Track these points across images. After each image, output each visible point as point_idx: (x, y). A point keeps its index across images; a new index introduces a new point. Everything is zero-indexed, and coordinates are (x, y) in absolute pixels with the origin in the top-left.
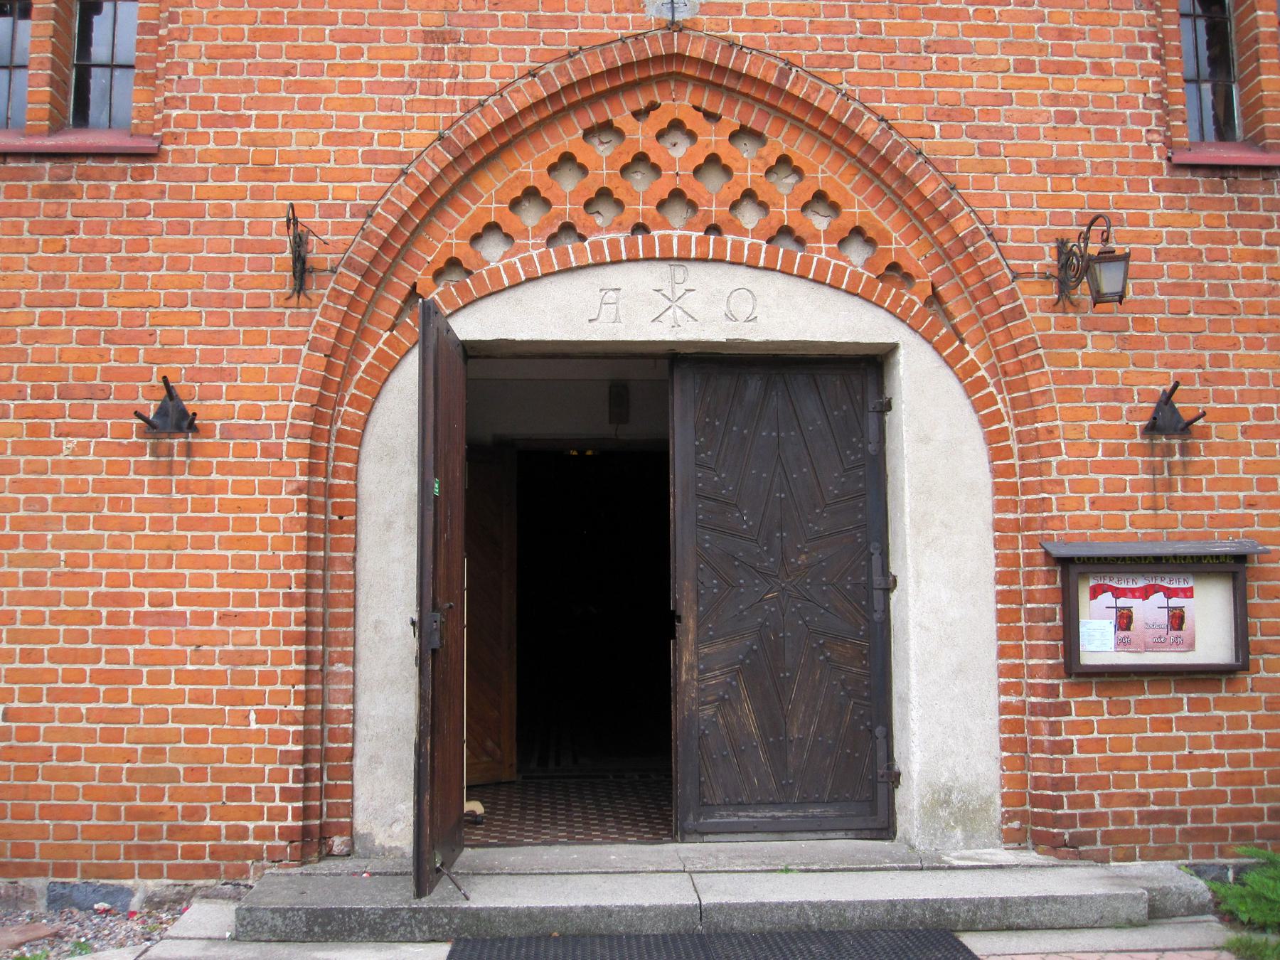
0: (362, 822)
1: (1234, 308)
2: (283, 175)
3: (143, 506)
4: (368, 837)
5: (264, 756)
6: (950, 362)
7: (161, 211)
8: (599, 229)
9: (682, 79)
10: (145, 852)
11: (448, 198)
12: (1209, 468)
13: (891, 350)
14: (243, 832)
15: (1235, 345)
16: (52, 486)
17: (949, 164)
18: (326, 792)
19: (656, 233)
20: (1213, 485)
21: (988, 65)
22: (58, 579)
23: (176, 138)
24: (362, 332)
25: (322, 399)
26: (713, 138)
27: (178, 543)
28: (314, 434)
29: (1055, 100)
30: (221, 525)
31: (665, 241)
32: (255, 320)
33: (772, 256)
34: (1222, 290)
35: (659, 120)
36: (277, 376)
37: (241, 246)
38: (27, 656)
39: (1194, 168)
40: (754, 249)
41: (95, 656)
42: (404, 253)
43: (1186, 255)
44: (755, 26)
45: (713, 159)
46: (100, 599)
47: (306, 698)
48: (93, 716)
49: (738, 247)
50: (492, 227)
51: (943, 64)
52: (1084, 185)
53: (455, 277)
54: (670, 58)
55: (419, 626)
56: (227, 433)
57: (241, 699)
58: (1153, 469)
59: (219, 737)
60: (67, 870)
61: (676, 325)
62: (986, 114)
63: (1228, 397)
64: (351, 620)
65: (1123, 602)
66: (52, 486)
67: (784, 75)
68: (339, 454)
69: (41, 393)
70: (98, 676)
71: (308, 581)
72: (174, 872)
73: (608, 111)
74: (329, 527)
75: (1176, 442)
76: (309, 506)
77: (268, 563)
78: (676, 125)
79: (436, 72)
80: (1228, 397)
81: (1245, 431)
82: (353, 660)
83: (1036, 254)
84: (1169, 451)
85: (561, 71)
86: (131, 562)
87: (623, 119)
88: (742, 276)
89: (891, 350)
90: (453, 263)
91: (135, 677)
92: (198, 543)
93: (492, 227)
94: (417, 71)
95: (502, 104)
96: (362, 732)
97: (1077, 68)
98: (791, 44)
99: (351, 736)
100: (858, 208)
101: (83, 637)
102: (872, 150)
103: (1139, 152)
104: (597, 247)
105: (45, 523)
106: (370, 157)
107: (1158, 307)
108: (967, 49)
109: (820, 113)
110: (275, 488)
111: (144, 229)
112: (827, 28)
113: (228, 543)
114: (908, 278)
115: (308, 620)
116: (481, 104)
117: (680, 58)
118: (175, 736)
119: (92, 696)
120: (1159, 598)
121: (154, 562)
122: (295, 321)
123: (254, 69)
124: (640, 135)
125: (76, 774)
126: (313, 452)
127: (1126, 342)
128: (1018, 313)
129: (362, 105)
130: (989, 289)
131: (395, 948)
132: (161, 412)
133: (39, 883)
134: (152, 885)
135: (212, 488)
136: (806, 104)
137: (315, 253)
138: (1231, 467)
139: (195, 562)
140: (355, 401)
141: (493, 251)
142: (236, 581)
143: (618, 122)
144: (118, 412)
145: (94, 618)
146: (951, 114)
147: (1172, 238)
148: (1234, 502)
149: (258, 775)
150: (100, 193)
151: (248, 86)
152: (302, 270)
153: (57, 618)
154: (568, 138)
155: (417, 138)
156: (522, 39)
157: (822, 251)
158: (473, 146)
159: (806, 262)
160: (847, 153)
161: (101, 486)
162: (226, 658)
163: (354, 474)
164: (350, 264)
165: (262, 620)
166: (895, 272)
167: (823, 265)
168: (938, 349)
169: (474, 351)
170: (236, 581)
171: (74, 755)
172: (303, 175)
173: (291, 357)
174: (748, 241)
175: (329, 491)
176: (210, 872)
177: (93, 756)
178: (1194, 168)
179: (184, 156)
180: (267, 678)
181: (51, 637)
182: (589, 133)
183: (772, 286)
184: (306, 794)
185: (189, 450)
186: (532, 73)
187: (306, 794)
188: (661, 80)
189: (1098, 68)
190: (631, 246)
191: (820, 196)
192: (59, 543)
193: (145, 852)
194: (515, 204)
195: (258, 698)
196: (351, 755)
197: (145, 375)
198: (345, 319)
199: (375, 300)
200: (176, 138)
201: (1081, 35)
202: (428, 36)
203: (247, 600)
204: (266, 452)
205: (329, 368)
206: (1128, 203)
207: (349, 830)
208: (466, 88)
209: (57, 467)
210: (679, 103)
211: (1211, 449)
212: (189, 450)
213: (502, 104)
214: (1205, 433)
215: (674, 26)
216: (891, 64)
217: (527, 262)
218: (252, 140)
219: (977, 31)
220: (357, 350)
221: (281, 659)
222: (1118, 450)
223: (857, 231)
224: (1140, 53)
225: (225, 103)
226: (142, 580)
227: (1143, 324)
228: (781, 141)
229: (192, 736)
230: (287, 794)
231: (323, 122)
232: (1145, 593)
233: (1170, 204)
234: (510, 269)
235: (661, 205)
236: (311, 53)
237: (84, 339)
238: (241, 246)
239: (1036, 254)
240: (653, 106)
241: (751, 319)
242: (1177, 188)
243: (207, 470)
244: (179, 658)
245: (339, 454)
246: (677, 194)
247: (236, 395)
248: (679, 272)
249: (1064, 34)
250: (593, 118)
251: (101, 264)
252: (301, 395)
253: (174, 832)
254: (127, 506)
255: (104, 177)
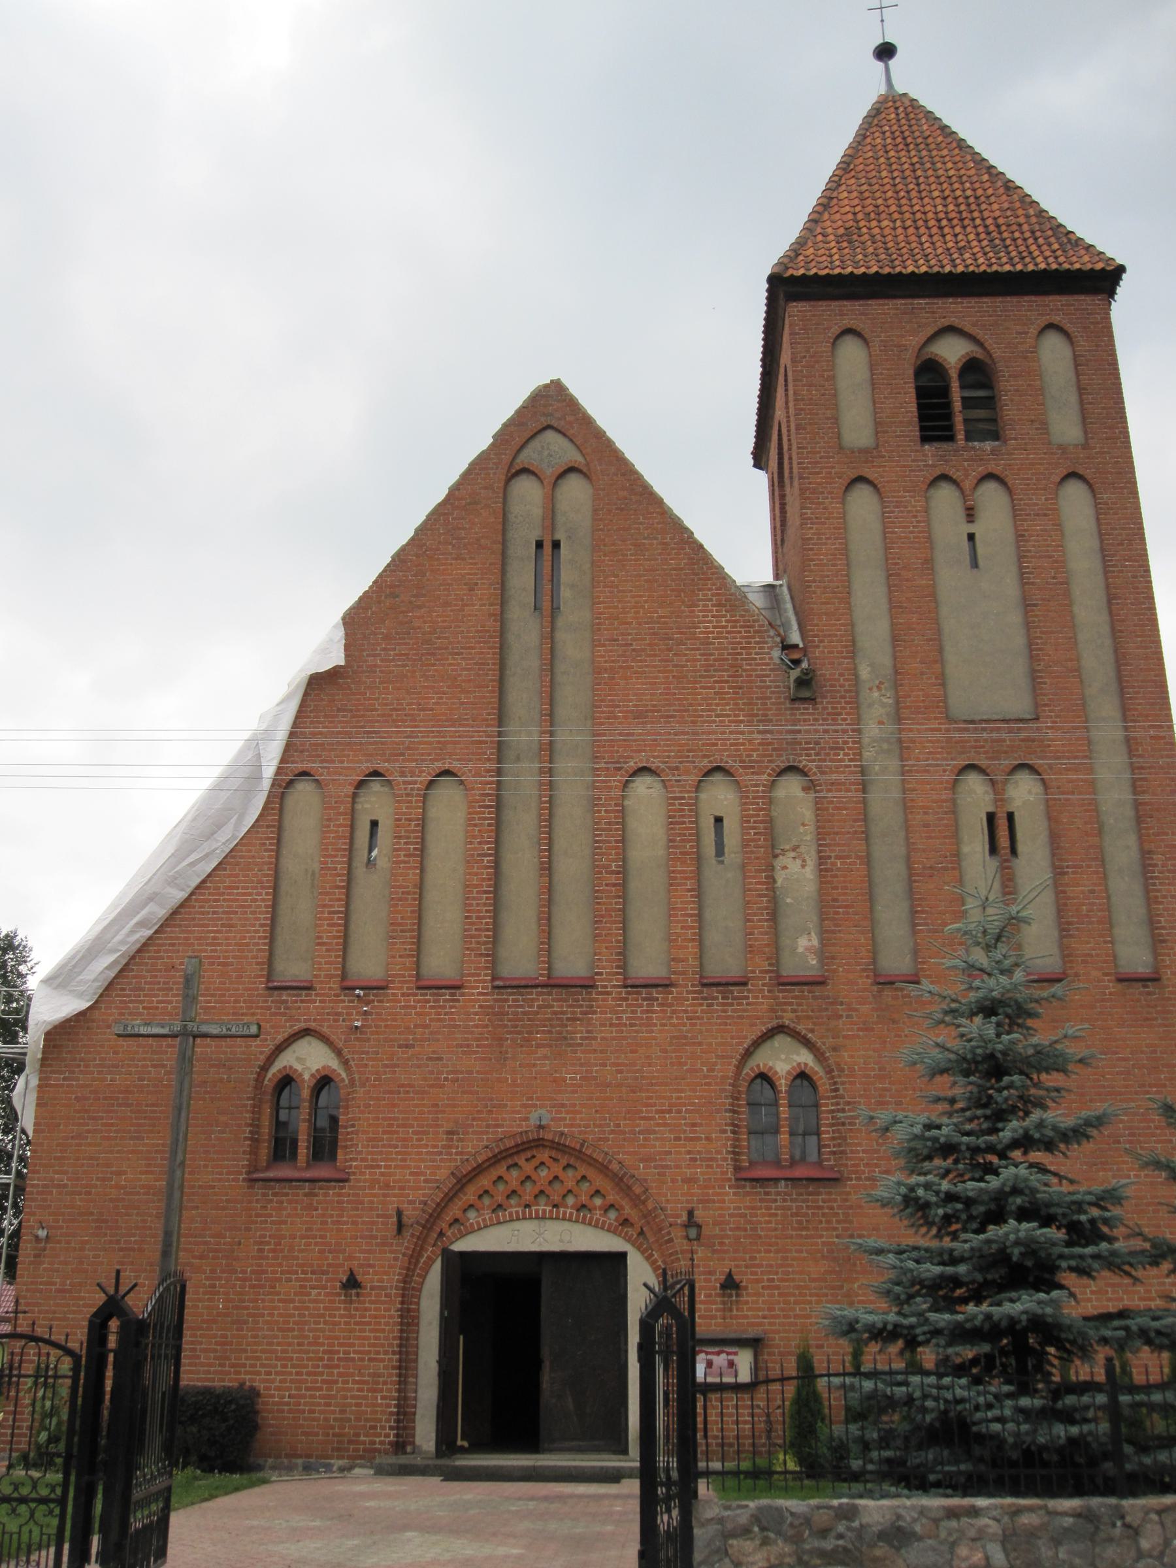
0: (418, 1441)
1: (760, 1237)
2: (393, 1188)
3: (341, 1316)
4: (420, 1447)
5: (383, 1413)
6: (647, 1258)
7: (348, 1202)
8: (511, 1206)
9: (544, 1146)
10: (338, 1450)
11: (456, 1194)
12: (747, 1302)
13: (622, 1256)
14: (374, 1443)
15: (759, 1252)
16: (307, 1308)
17: (646, 1180)
18: (405, 1428)
19: (533, 1208)
20: (749, 1309)
21: (663, 1139)
22: (310, 1344)
23: (354, 1173)
24: (422, 1248)
25: (407, 1275)
26: (557, 1169)
27: (354, 1330)
28: (404, 1289)
29: (689, 1152)
30: (369, 1323)
31: (537, 1211)
32: (383, 1244)
33: (578, 1216)
34: (755, 1229)
35: (535, 1162)
36: (390, 1266)
37: (378, 1216)
38: (297, 1373)
39: (745, 1180)
40: (571, 1214)
41: (322, 1374)
42: (438, 1217)
43: (741, 1215)
44: (572, 1126)
45: (556, 1178)
46: (324, 1352)
47: (399, 1391)
48: (321, 1397)
49: (564, 1213)
50: (471, 1206)
51: (645, 1139)
52: (700, 1187)
53: (457, 1226)
54: (539, 1139)
55: (439, 1362)
56: (372, 1288)
57: (375, 1391)
58: (724, 1303)
59: (366, 1405)
60: (309, 1456)
61: (540, 1244)
62: (661, 1159)
63: (756, 1273)
64: (416, 1361)
65: (709, 1357)
66: (307, 1308)
67: (582, 1145)
68: (413, 1296)
69: (304, 1272)
70: (323, 1381)
71: (400, 1346)
72: (349, 1458)
73: (516, 1159)
74: (408, 1324)
75: (734, 1292)
76: (401, 1316)
77: (386, 1338)
78: (542, 1163)
79: (450, 1147)
80: (756, 1273)
81: (763, 1287)
82: (416, 1377)
83: (678, 1216)
84: (731, 1296)
85: (498, 1146)
86: (337, 1338)
87: (522, 1162)
88: (567, 1225)
89: (622, 1256)
90: (456, 1220)
91: (336, 1382)
92: (360, 1331)
93: (471, 1206)
94: (444, 1147)
95: (475, 1159)
96: (419, 1405)
97: (699, 1139)
98: (585, 1133)
99: (415, 1406)
100: (612, 1197)
101: (318, 1366)
102: (616, 1175)
103: (723, 1173)
104: (511, 1214)
105: (305, 1323)
106: (426, 1181)
107: (728, 1237)
108: (655, 1132)
109: (596, 1160)
110: (389, 1310)
111: (342, 1209)
112: (600, 1126)
113: (371, 1331)
114: (632, 1225)
115: (400, 1360)
116: (467, 1160)
117: (543, 1139)
118: (350, 1405)
119: (321, 1389)
120: (723, 1356)
121: (344, 1338)
122: (397, 1245)
123: (383, 1146)
124: (528, 1168)
125: (314, 1419)
126: (403, 1296)
127: (714, 1251)
128: (671, 1240)
129: (423, 1161)
130: (661, 1230)
131: (95, 994)
132: (348, 1280)
133: (300, 1461)
134: (341, 1462)
135: (366, 1309)
136: (590, 1157)
137: (405, 1220)
138: (757, 1302)
139: (359, 1338)
140: (419, 1275)
141: (472, 1214)
142: (374, 1345)
143: (520, 1163)
144: (332, 1280)
145: (322, 1359)
146: (646, 1160)
147: (735, 1208)
148: (758, 1317)
149: (380, 1420)
150: (326, 1195)
151: (381, 1153)
152: (400, 1227)
153: (309, 1359)
154: (501, 1170)
155: (443, 1174)
156: (482, 1133)
157: (598, 1214)
158: (465, 1176)
159: (591, 1218)
160: (607, 1176)
161: (325, 1308)
162: (369, 1375)
163: (418, 1304)
164: (418, 1223)
165: (382, 1360)
166: (626, 1222)
167: (598, 1220)
168: (643, 1253)
169: (463, 1255)
170: (374, 1345)
171: (313, 1412)
172: (401, 1188)
173: (396, 1259)
174: (568, 1211)
175: (409, 1310)
176: (361, 1458)
177: (321, 1412)
178: (745, 1180)
179: (358, 1181)
180: (385, 1383)
181: (306, 1366)
182: (508, 1168)
183: (578, 1229)
184: (398, 1428)
185: (358, 1295)
186: (487, 1147)
187: (398, 1428)
188: (537, 1146)
189: (708, 1139)
190: (524, 1213)
191: (597, 1192)
192: (310, 1330)
193: (338, 1450)
194: (480, 1197)
195: (381, 1390)
196: (414, 1414)
197: (342, 1265)
198: (416, 1244)
199: (427, 1236)
200: (354, 1173)
201: (701, 1125)
202: (448, 1133)
203: (378, 1353)
204: (386, 1296)
205: (410, 1263)
206: (719, 1194)
207: (413, 1443)
208: (461, 1153)
209: (310, 1301)
210: (544, 1155)
211: (748, 1295)
212: (358, 1295)
213: (475, 1159)
214: (746, 1288)
215: (540, 1127)
216: (624, 1140)
217: (484, 1220)
218: (382, 1174)
219: (658, 1125)
220: (420, 1255)
221: (390, 1375)
222: (710, 1295)
223: (612, 1206)
224: (725, 1132)
225: (373, 1160)
226: (340, 1345)
227: (722, 1244)
228: (583, 1170)
229: (357, 1405)
230: (391, 1428)
231: (408, 1167)
232: (718, 1353)
233: (735, 1194)
234: (478, 1223)
235: (536, 1196)
236: (404, 1140)
237: (320, 1252)
238: (378, 1216)
239: (678, 1216)
240: (534, 1157)
241: (570, 1242)
242: (738, 1187)
243: (364, 1302)
244: (353, 1375)
245: (413, 1296)
246: (542, 1192)
247: (376, 1273)
248: (542, 1223)
249: (694, 1125)
250: (510, 1162)
251: (326, 1223)
252: (399, 1274)
253: (350, 1442)
254: (335, 1316)
255: (328, 1188)
